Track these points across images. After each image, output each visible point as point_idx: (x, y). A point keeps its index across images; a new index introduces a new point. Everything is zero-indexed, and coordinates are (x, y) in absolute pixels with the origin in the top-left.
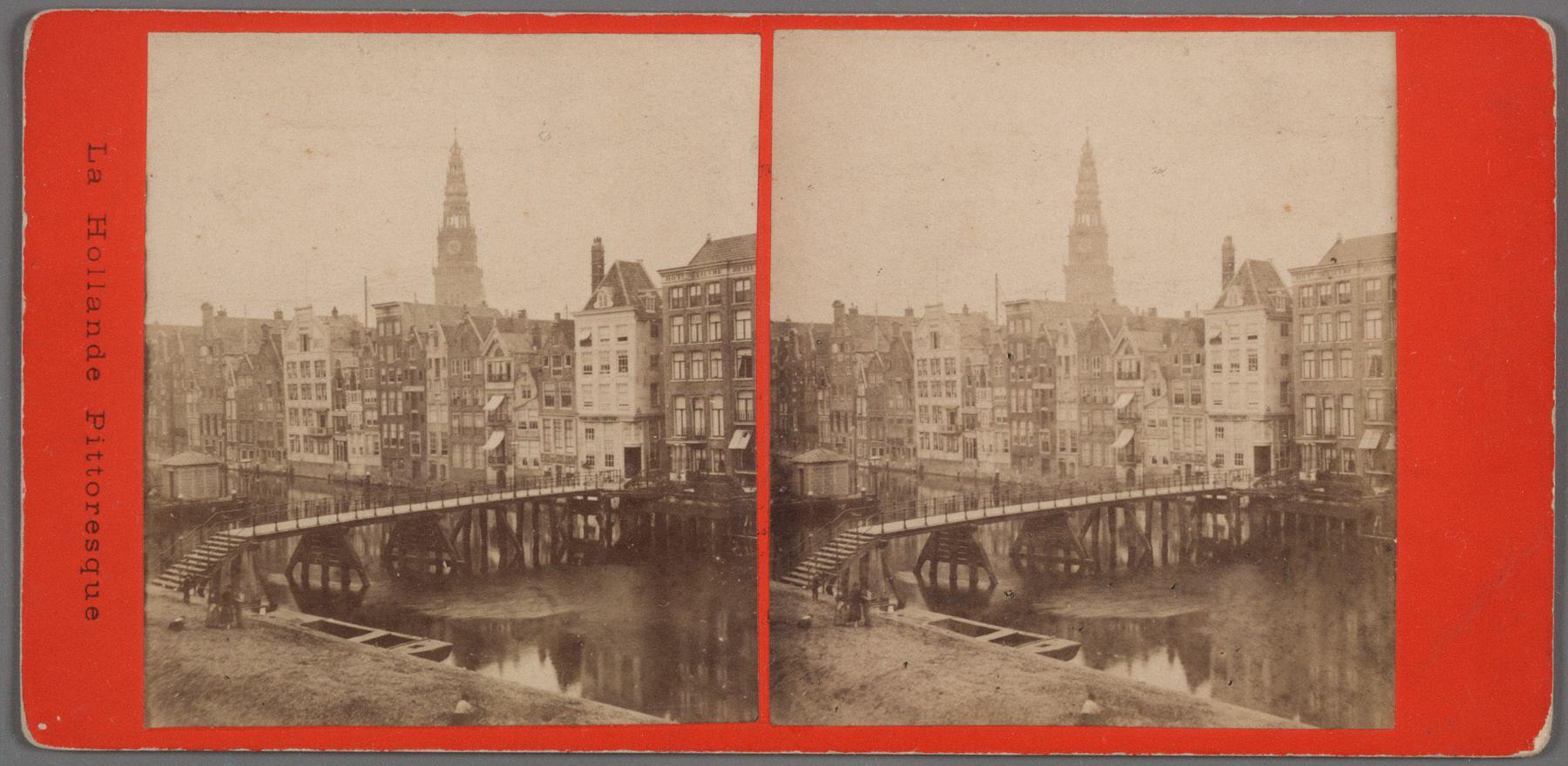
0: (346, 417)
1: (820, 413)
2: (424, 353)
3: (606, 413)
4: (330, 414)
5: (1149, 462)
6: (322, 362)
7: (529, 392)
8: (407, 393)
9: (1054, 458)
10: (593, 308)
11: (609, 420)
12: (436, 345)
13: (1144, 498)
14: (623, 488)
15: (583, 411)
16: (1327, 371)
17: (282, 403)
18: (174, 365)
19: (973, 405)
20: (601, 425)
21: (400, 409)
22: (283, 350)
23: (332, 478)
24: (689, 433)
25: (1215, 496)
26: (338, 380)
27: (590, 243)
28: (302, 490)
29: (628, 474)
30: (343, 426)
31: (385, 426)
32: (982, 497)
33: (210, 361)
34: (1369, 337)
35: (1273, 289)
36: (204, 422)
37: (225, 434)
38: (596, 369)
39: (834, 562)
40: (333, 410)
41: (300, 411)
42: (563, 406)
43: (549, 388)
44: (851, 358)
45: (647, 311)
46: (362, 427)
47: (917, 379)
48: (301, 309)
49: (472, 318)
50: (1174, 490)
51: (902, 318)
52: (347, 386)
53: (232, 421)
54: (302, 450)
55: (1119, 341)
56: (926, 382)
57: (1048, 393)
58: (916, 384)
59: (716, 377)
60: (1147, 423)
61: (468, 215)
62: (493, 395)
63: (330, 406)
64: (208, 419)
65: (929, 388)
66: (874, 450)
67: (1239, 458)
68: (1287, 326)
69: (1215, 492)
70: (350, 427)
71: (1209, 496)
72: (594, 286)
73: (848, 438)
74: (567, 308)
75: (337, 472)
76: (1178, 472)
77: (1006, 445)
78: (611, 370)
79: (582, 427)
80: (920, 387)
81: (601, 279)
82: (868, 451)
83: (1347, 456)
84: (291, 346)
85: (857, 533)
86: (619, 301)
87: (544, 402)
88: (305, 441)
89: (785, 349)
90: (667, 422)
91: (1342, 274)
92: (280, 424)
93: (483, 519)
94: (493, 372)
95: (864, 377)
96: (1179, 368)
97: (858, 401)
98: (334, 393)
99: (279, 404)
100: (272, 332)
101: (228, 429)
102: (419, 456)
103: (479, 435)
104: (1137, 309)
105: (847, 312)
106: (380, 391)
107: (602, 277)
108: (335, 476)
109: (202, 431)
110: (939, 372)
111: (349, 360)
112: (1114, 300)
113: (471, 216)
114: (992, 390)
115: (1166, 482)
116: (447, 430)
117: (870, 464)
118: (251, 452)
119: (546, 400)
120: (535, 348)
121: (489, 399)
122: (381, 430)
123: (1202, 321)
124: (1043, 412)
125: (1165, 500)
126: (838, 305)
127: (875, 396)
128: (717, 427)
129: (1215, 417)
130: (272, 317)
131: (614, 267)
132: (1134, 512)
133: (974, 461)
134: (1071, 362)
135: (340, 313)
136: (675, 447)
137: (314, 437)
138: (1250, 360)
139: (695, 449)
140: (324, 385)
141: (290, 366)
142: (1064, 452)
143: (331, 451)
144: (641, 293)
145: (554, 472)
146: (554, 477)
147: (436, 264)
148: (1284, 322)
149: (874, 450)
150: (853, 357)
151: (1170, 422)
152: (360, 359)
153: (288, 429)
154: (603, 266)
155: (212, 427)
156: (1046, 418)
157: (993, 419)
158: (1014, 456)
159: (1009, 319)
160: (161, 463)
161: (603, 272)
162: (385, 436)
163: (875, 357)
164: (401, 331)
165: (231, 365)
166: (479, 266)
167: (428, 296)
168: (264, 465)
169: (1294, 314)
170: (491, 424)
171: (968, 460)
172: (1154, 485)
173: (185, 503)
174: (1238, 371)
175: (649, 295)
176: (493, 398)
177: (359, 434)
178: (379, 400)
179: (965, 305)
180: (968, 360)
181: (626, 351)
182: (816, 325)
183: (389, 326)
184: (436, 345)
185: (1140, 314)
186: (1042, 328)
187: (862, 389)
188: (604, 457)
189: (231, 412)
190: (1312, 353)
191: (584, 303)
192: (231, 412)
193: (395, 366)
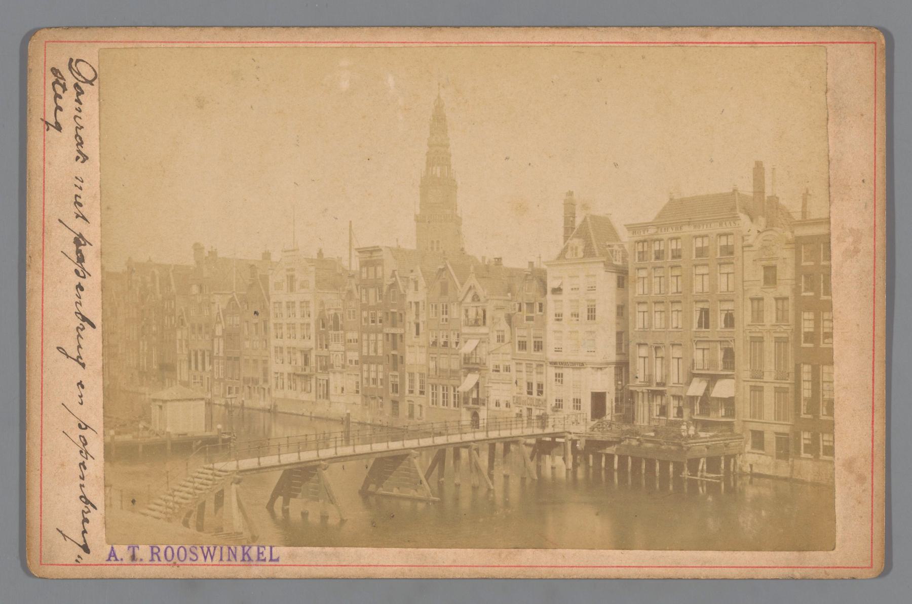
0: (329, 356)
2: (403, 296)
5: (492, 406)
6: (307, 302)
10: (565, 258)
15: (552, 356)
16: (658, 321)
19: (327, 347)
21: (380, 351)
26: (323, 322)
34: (722, 290)
39: (190, 496)
40: (316, 348)
50: (516, 432)
52: (331, 326)
59: (677, 327)
62: (469, 339)
63: (313, 346)
64: (196, 355)
70: (332, 366)
71: (548, 439)
72: (566, 238)
74: (540, 257)
76: (519, 415)
77: (357, 387)
80: (276, 329)
81: (572, 231)
83: (676, 402)
86: (589, 252)
87: (517, 346)
90: (631, 369)
92: (265, 362)
95: (222, 317)
97: (216, 341)
101: (216, 366)
102: (397, 395)
104: (484, 258)
122: (361, 370)
124: (393, 355)
125: (508, 443)
126: (198, 248)
127: (231, 336)
129: (555, 363)
133: (327, 402)
134: (421, 308)
142: (411, 395)
147: (418, 212)
148: (620, 275)
155: (200, 361)
156: (397, 362)
157: (345, 361)
162: (365, 375)
164: (383, 274)
165: (220, 303)
176: (469, 341)
177: (341, 373)
183: (372, 269)
185: (486, 263)
186: (393, 276)
191: (556, 252)
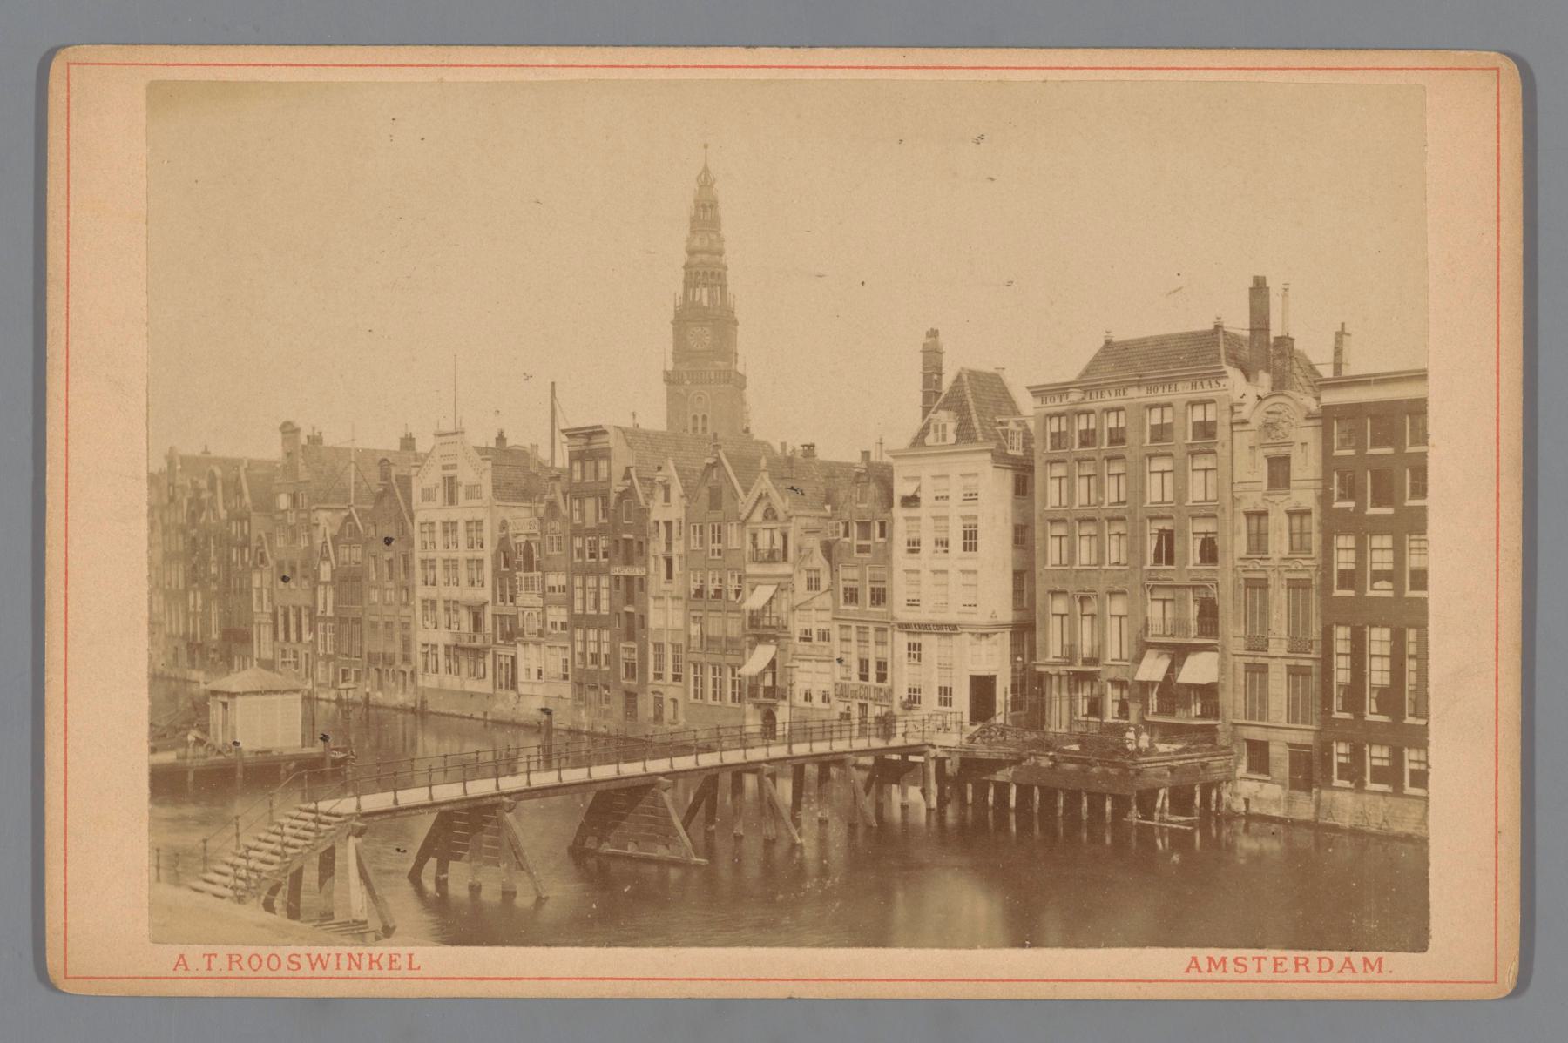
1: (255, 610)
2: (645, 511)
4: (489, 610)
6: (480, 523)
7: (818, 580)
8: (617, 578)
9: (644, 692)
11: (948, 630)
14: (965, 742)
17: (408, 589)
19: (512, 600)
20: (933, 639)
22: (414, 503)
23: (489, 717)
24: (1070, 655)
25: (905, 757)
26: (505, 553)
28: (440, 735)
29: (975, 718)
31: (579, 634)
32: (524, 753)
35: (1004, 419)
36: (281, 620)
37: (313, 643)
38: (927, 546)
42: (872, 605)
43: (848, 574)
44: (309, 519)
46: (541, 634)
48: (446, 434)
49: (727, 455)
50: (840, 746)
51: (395, 452)
52: (519, 565)
53: (325, 619)
54: (442, 667)
56: (434, 560)
58: (417, 563)
59: (1118, 564)
61: (723, 287)
63: (489, 598)
66: (345, 672)
67: (946, 695)
69: (906, 751)
70: (521, 633)
72: (926, 411)
73: (302, 654)
76: (846, 716)
78: (923, 548)
79: (902, 640)
80: (424, 568)
82: (336, 673)
84: (428, 496)
86: (965, 433)
92: (406, 626)
96: (851, 545)
99: (404, 592)
100: (394, 472)
104: (783, 445)
105: (304, 441)
106: (573, 572)
110: (456, 543)
111: (522, 520)
112: (747, 431)
115: (827, 733)
116: (681, 640)
119: (873, 597)
120: (828, 507)
121: (753, 590)
122: (572, 640)
125: (825, 763)
126: (289, 430)
128: (1115, 649)
129: (908, 626)
130: (396, 447)
131: (959, 378)
132: (774, 783)
133: (512, 695)
135: (510, 443)
136: (1051, 676)
141: (425, 528)
143: (490, 673)
144: (1001, 423)
146: (856, 721)
148: (1022, 473)
149: (345, 672)
151: (835, 634)
152: (541, 519)
153: (419, 633)
156: (633, 627)
158: (579, 684)
160: (207, 687)
163: (350, 517)
164: (609, 474)
166: (740, 369)
167: (654, 419)
168: (379, 694)
169: (1036, 459)
170: (755, 631)
171: (501, 693)
175: (1012, 426)
177: (537, 644)
183: (590, 465)
185: (788, 454)
188: (937, 690)
190: (1064, 525)
193: (599, 531)
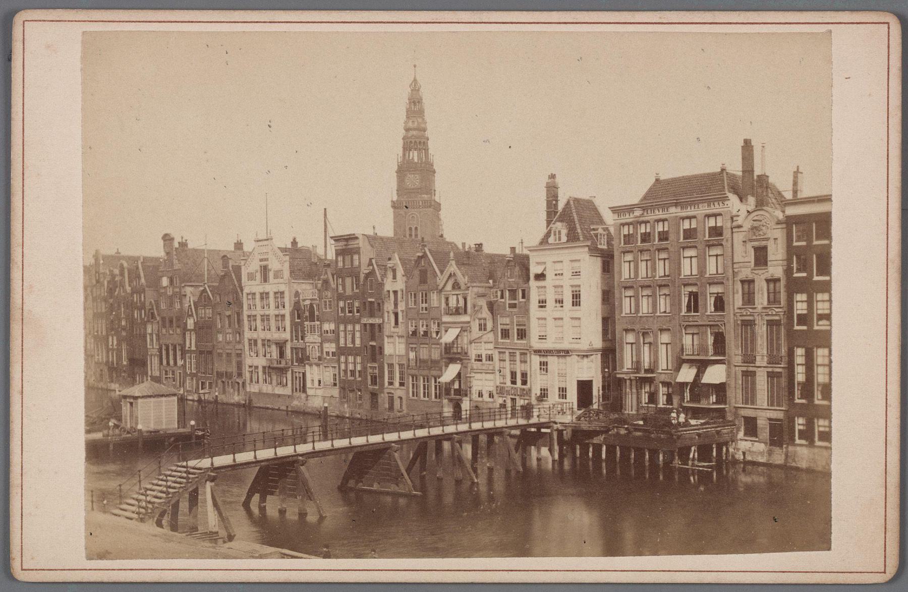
2: (381, 285)
3: (559, 346)
4: (289, 346)
5: (475, 396)
6: (282, 293)
7: (485, 325)
12: (394, 277)
13: (471, 431)
15: (536, 344)
16: (645, 307)
17: (240, 333)
18: (135, 296)
26: (297, 309)
27: (545, 180)
30: (302, 358)
31: (343, 359)
33: (170, 292)
36: (164, 353)
38: (550, 303)
41: (260, 343)
43: (503, 321)
45: (599, 246)
46: (320, 358)
47: (246, 312)
50: (500, 424)
53: (191, 352)
54: (261, 380)
55: (447, 277)
57: (377, 327)
60: (474, 357)
61: (427, 150)
65: (259, 322)
68: (608, 262)
70: (308, 358)
72: (549, 222)
75: (295, 403)
84: (251, 277)
85: (186, 467)
86: (573, 237)
88: (264, 373)
89: (116, 282)
91: (661, 213)
92: (239, 355)
93: (439, 449)
94: (450, 305)
98: (293, 324)
100: (231, 263)
103: (435, 366)
104: (464, 244)
107: (556, 213)
108: (292, 407)
109: (161, 363)
111: (307, 291)
113: (430, 151)
114: (321, 324)
115: (492, 416)
117: (200, 397)
118: (210, 383)
119: (502, 334)
120: (491, 281)
121: (446, 331)
122: (339, 361)
123: (527, 257)
126: (168, 239)
127: (204, 329)
128: (664, 363)
129: (539, 351)
137: (274, 368)
138: (573, 295)
139: (645, 383)
140: (283, 316)
141: (250, 297)
144: (594, 229)
145: (509, 404)
146: (510, 409)
150: (183, 291)
154: (557, 201)
156: (376, 353)
157: (322, 353)
158: (343, 389)
159: (338, 253)
160: (122, 393)
161: (557, 209)
170: (447, 356)
171: (297, 394)
172: (481, 418)
173: (145, 434)
174: (562, 307)
178: (336, 332)
179: (294, 239)
180: (297, 294)
181: (579, 286)
182: (145, 258)
184: (394, 277)
187: (190, 323)
189: (191, 344)
192: (191, 344)
